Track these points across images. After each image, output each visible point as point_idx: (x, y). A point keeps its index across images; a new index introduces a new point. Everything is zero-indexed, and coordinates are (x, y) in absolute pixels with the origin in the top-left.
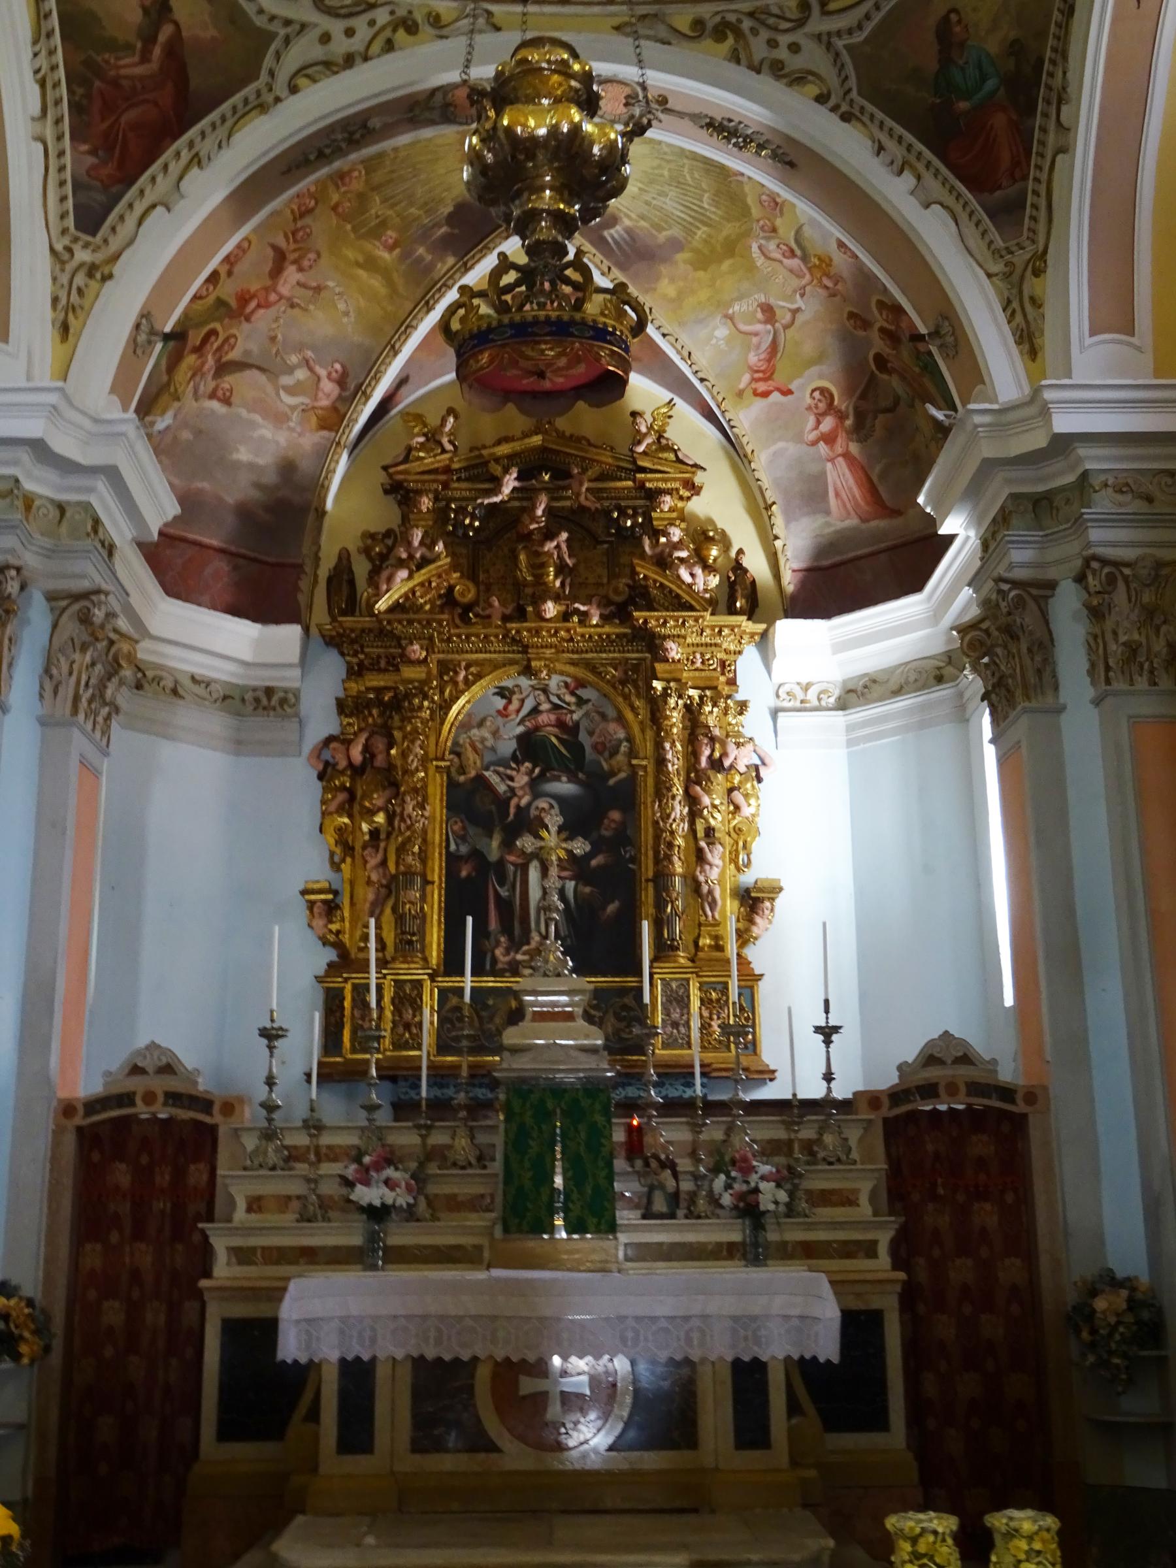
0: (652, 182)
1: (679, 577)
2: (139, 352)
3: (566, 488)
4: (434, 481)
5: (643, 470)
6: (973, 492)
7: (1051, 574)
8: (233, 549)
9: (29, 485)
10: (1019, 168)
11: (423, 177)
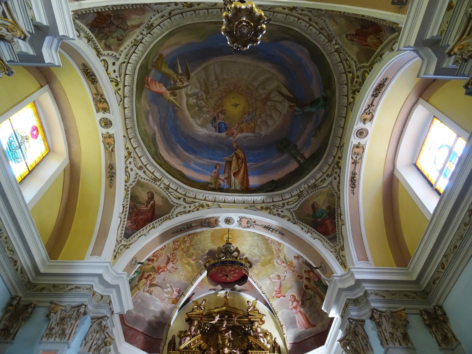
0: (252, 246)
1: (260, 341)
2: (132, 266)
3: (232, 320)
4: (199, 317)
5: (250, 315)
6: (337, 301)
7: (363, 318)
8: (145, 333)
9: (95, 289)
10: (334, 230)
11: (202, 244)
